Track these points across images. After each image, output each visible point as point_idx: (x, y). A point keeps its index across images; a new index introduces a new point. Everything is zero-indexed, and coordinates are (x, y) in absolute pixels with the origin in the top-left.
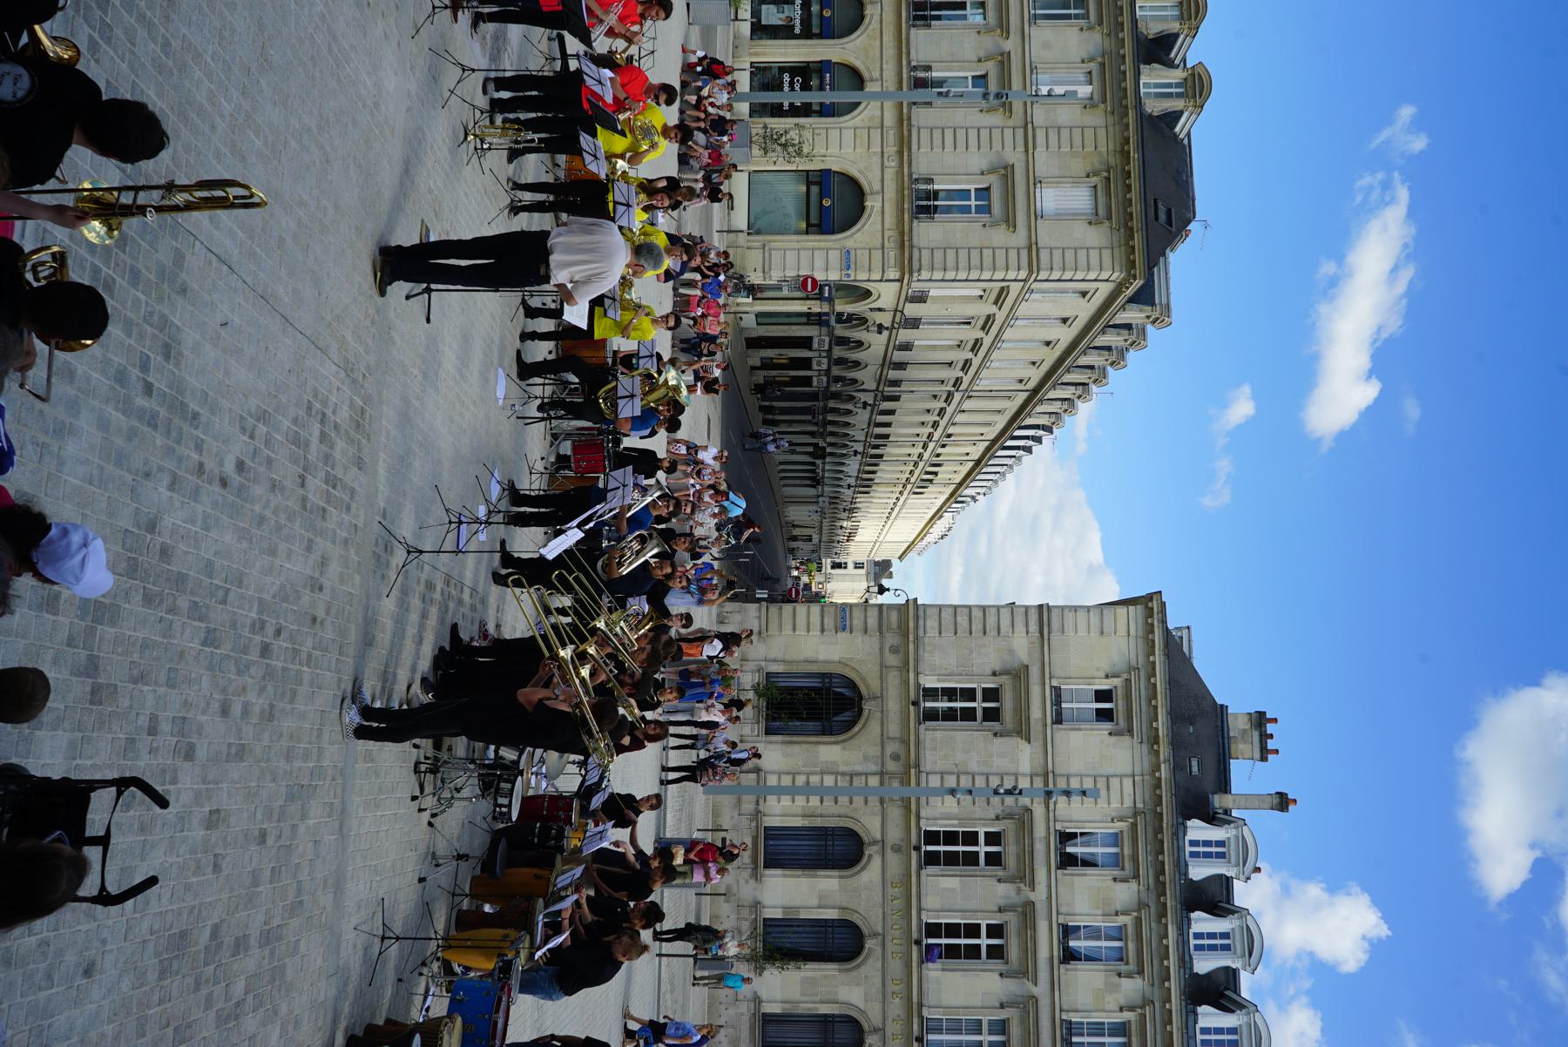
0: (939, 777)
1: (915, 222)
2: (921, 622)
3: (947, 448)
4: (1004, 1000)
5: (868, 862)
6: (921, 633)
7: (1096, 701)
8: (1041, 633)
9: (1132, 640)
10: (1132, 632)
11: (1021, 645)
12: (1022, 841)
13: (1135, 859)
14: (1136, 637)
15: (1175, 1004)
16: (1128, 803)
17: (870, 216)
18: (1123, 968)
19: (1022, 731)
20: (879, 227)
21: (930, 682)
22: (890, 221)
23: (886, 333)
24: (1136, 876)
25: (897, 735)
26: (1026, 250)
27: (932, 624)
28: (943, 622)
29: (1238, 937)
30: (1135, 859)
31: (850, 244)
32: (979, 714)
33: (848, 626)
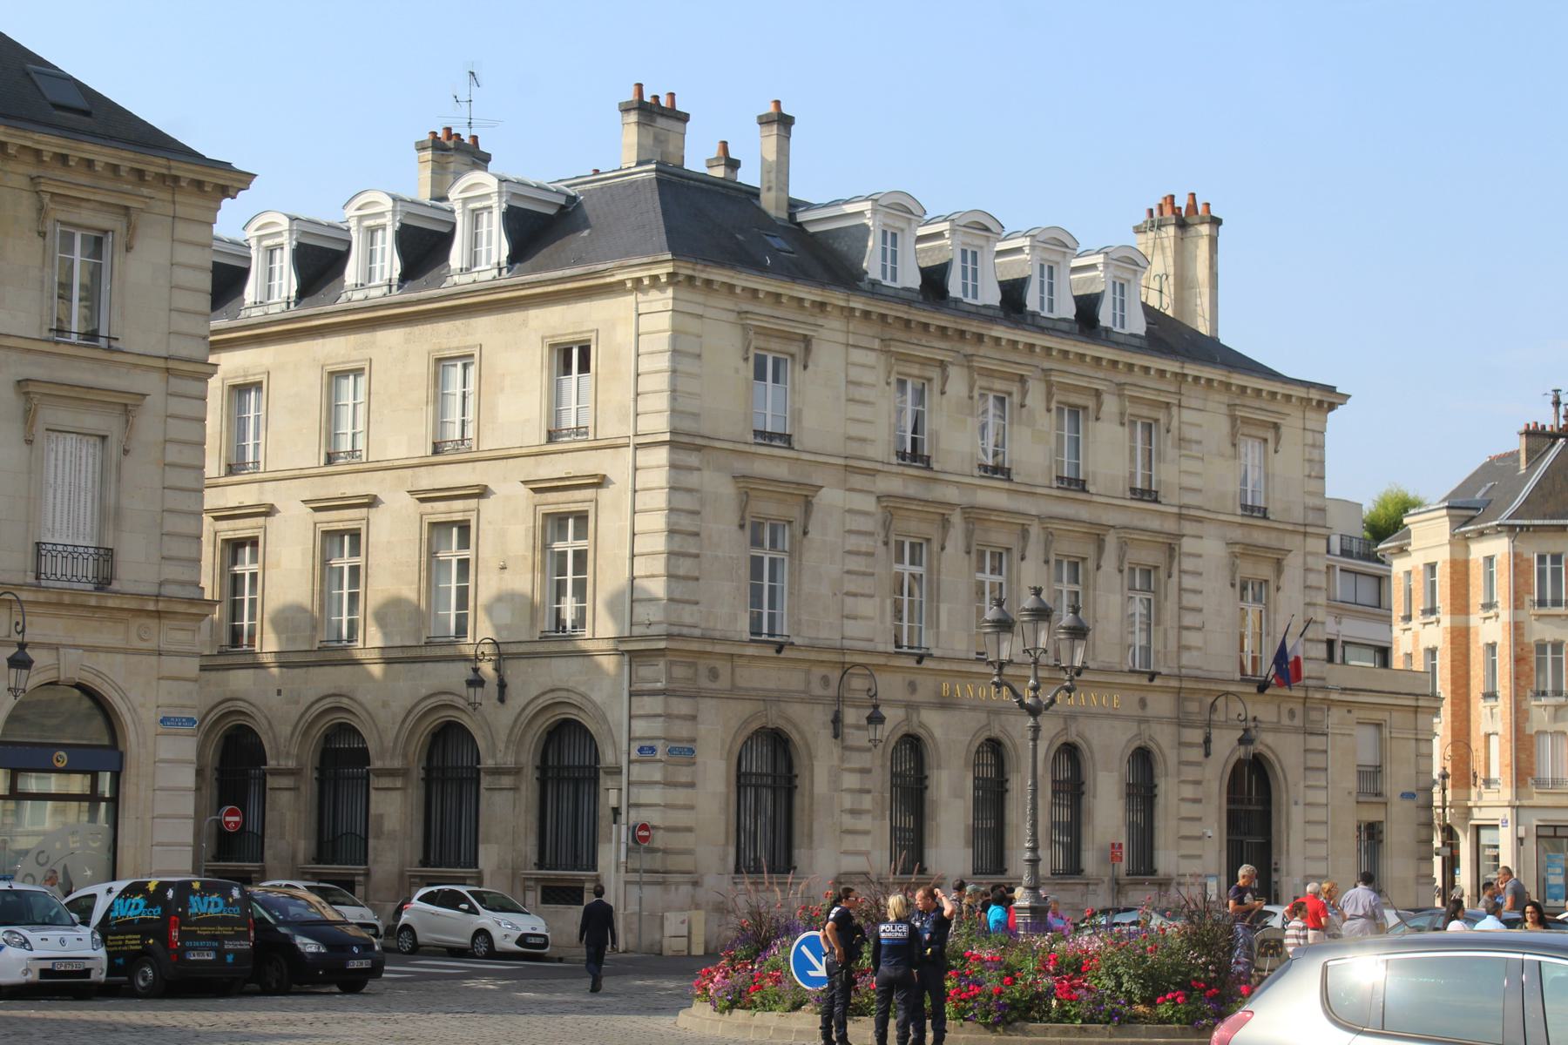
0: (1185, 633)
1: (115, 586)
2: (685, 631)
3: (884, 548)
4: (1042, 558)
5: (788, 720)
6: (697, 632)
7: (765, 380)
8: (699, 448)
9: (709, 313)
10: (699, 310)
11: (718, 485)
12: (908, 513)
13: (925, 362)
14: (705, 306)
15: (1022, 337)
16: (871, 358)
17: (98, 674)
18: (1016, 399)
19: (806, 498)
20: (119, 658)
21: (743, 627)
22: (108, 635)
23: (884, 711)
24: (942, 365)
25: (741, 683)
26: (172, 380)
27: (688, 615)
28: (686, 597)
29: (968, 240)
30: (925, 362)
31: (150, 716)
32: (757, 552)
33: (688, 746)
